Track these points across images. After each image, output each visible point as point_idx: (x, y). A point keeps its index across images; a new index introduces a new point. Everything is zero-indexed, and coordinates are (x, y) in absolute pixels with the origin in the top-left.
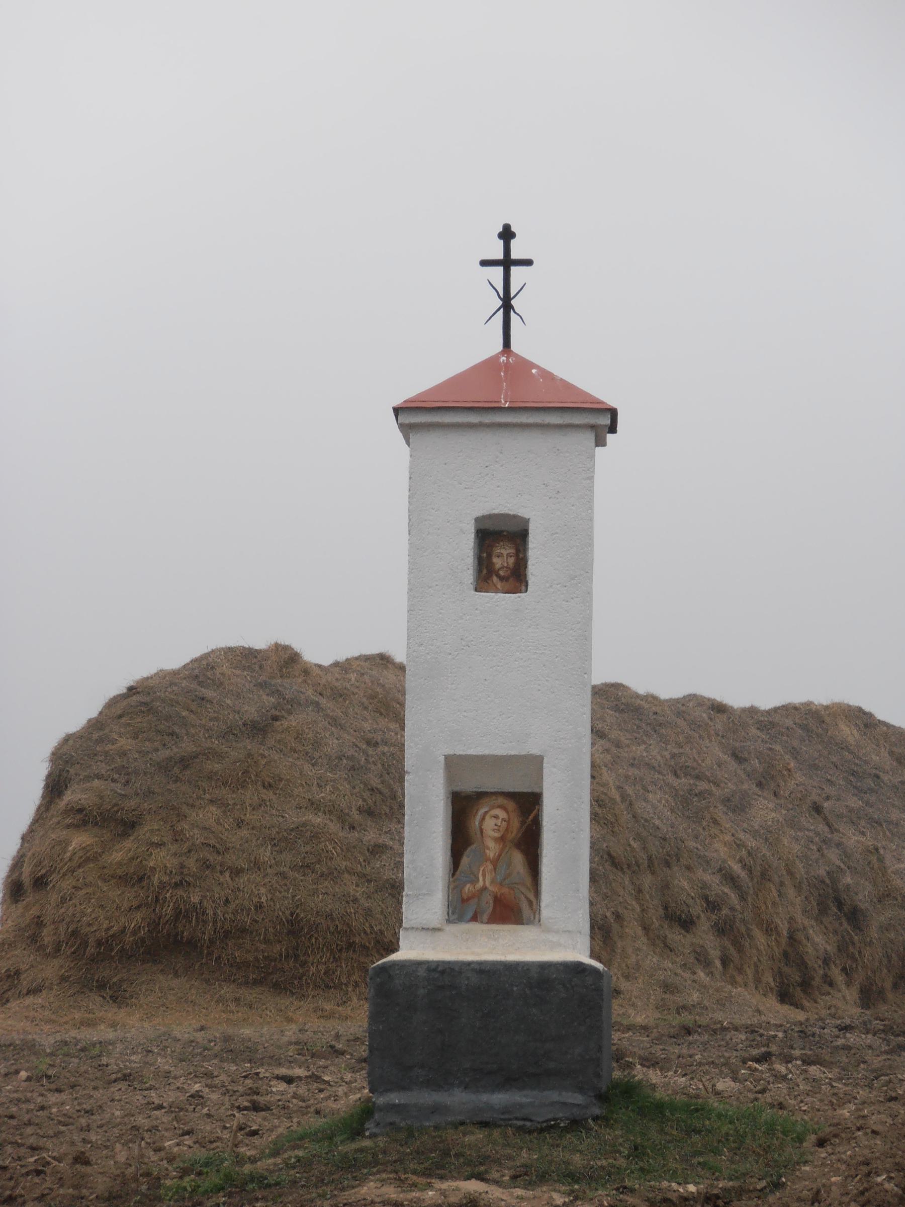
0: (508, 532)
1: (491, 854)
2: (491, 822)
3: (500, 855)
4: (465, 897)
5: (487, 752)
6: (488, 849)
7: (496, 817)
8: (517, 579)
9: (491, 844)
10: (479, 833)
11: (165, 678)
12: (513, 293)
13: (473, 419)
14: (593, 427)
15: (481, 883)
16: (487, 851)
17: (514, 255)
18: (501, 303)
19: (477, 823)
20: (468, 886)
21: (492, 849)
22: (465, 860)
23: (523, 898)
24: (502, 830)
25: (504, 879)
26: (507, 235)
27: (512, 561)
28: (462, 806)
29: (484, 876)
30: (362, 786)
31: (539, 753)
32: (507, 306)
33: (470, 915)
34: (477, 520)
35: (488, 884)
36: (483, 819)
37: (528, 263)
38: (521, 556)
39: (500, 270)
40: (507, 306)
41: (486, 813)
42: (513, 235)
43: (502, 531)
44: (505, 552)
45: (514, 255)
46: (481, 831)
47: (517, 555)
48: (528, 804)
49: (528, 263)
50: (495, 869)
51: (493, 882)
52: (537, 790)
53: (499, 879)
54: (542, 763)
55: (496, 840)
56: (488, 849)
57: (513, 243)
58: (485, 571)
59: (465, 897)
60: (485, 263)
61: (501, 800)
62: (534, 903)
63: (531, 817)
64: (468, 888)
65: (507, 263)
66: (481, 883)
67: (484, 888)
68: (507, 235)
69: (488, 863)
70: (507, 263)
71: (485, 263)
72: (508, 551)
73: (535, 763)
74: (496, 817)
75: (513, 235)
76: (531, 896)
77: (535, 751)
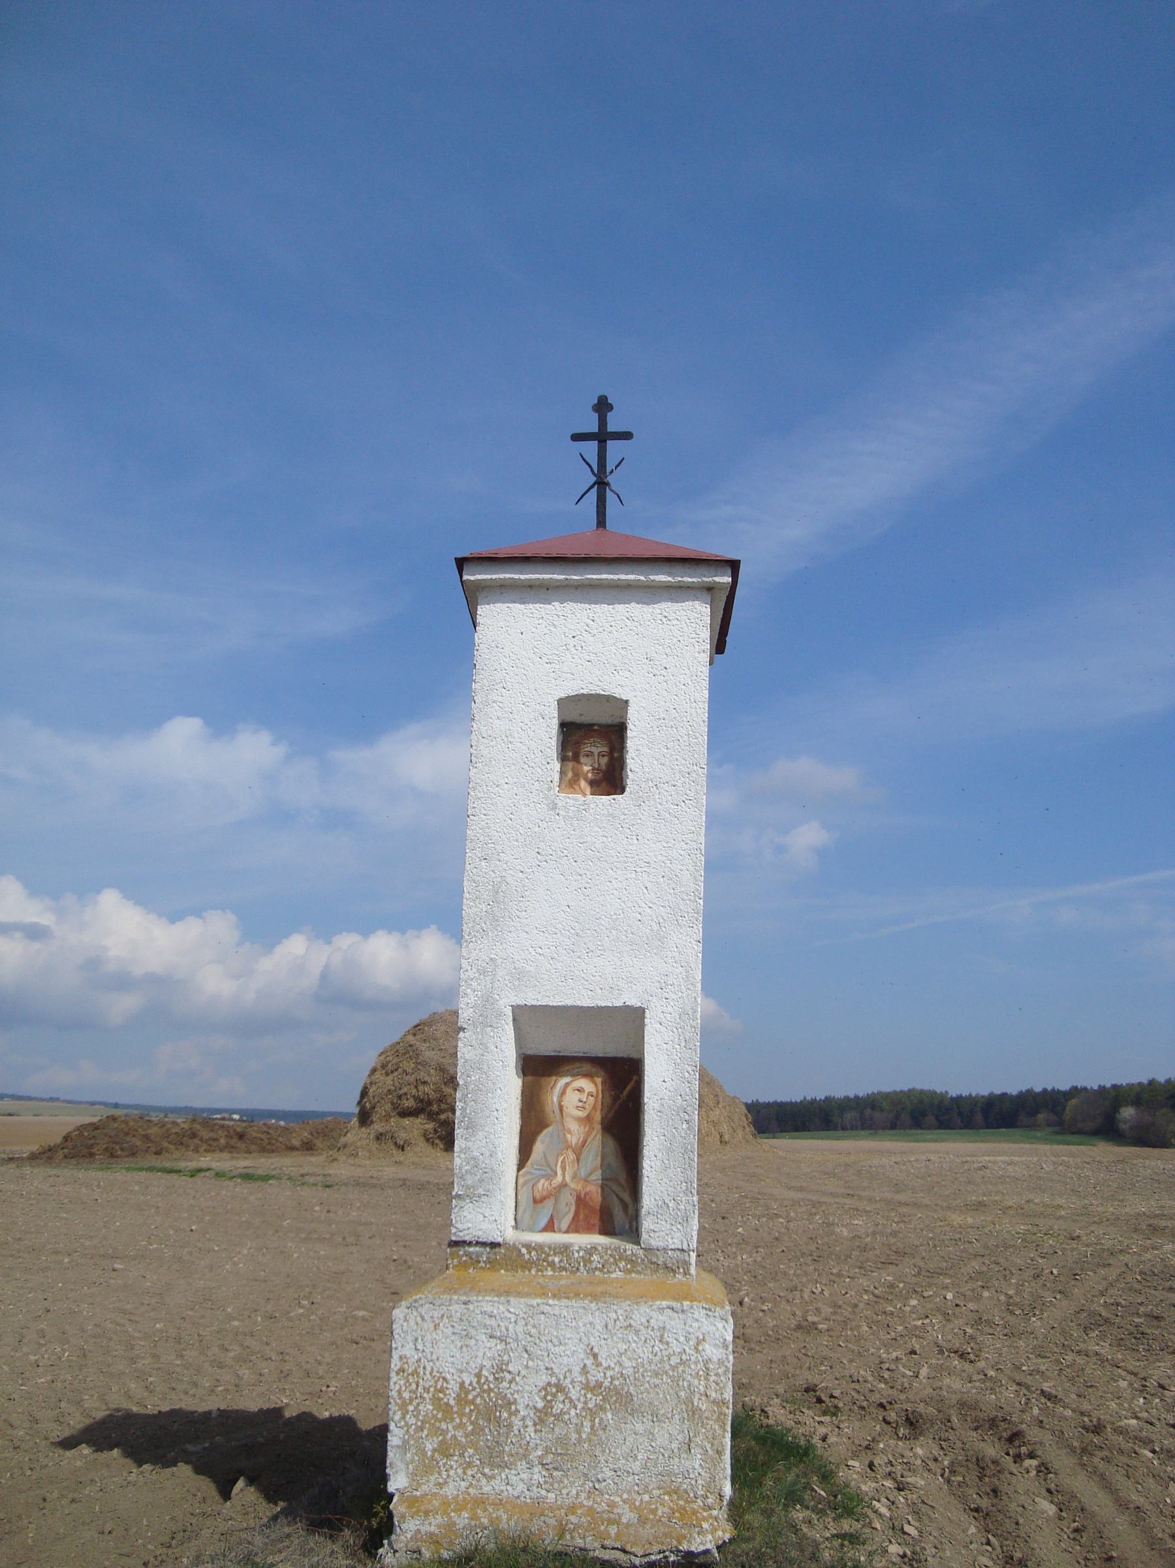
0: (599, 725)
1: (573, 1139)
2: (576, 1097)
3: (585, 1142)
4: (538, 1197)
5: (569, 1003)
6: (570, 1132)
7: (580, 1090)
8: (611, 780)
9: (573, 1126)
10: (557, 1111)
11: (611, 1522)
12: (610, 466)
13: (556, 576)
14: (710, 589)
15: (559, 1178)
16: (569, 1136)
17: (611, 428)
18: (594, 479)
19: (555, 1099)
20: (542, 1181)
21: (575, 1132)
22: (539, 1148)
23: (615, 1198)
24: (588, 1107)
25: (591, 1173)
26: (603, 406)
27: (604, 761)
28: (538, 1068)
29: (564, 1169)
30: (422, 1221)
31: (639, 1004)
32: (601, 484)
33: (543, 1222)
34: (560, 701)
35: (568, 1179)
36: (563, 1093)
37: (627, 436)
38: (616, 755)
39: (594, 445)
40: (601, 484)
41: (567, 1084)
42: (610, 407)
43: (594, 725)
44: (596, 751)
45: (611, 428)
46: (561, 1108)
47: (611, 753)
48: (622, 1078)
49: (627, 436)
50: (578, 1160)
51: (575, 1176)
52: (635, 1055)
53: (583, 1173)
54: (643, 1017)
55: (579, 1120)
56: (570, 1132)
57: (610, 416)
58: (570, 774)
59: (538, 1197)
60: (577, 437)
61: (587, 1067)
62: (630, 1206)
63: (625, 1093)
64: (542, 1185)
65: (602, 437)
66: (559, 1178)
67: (564, 1185)
68: (603, 406)
69: (570, 1152)
70: (602, 437)
71: (577, 437)
72: (600, 749)
73: (634, 1017)
74: (580, 1090)
75: (610, 407)
76: (626, 1197)
77: (633, 1002)
